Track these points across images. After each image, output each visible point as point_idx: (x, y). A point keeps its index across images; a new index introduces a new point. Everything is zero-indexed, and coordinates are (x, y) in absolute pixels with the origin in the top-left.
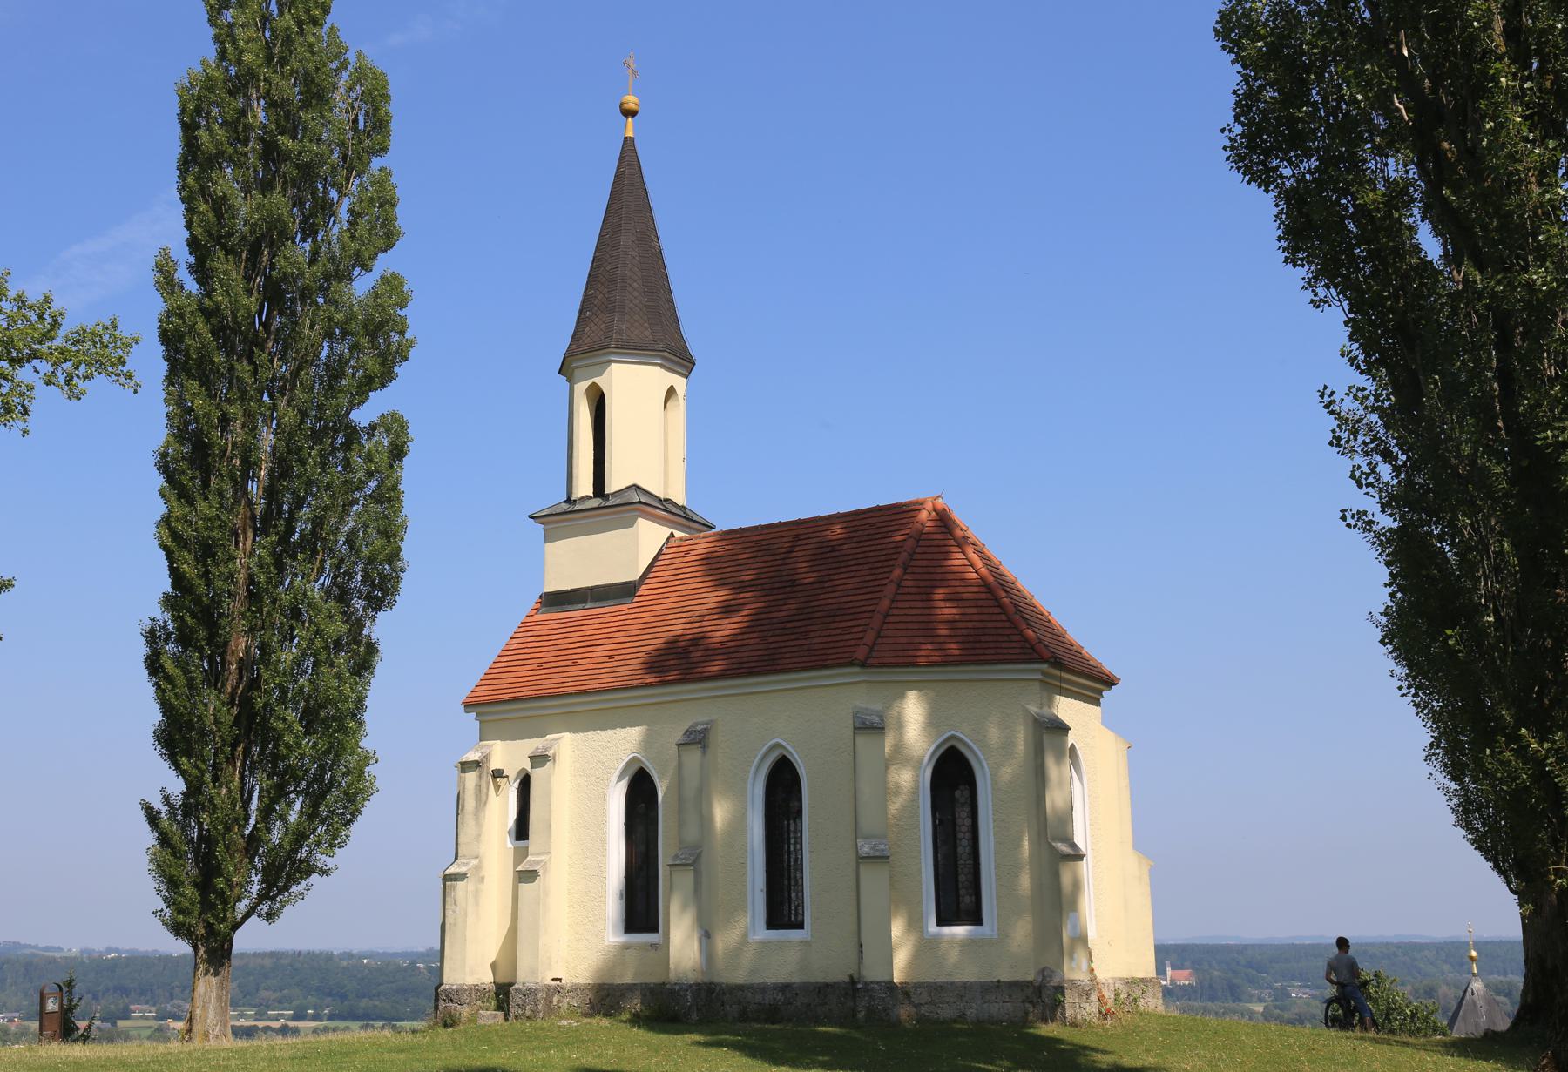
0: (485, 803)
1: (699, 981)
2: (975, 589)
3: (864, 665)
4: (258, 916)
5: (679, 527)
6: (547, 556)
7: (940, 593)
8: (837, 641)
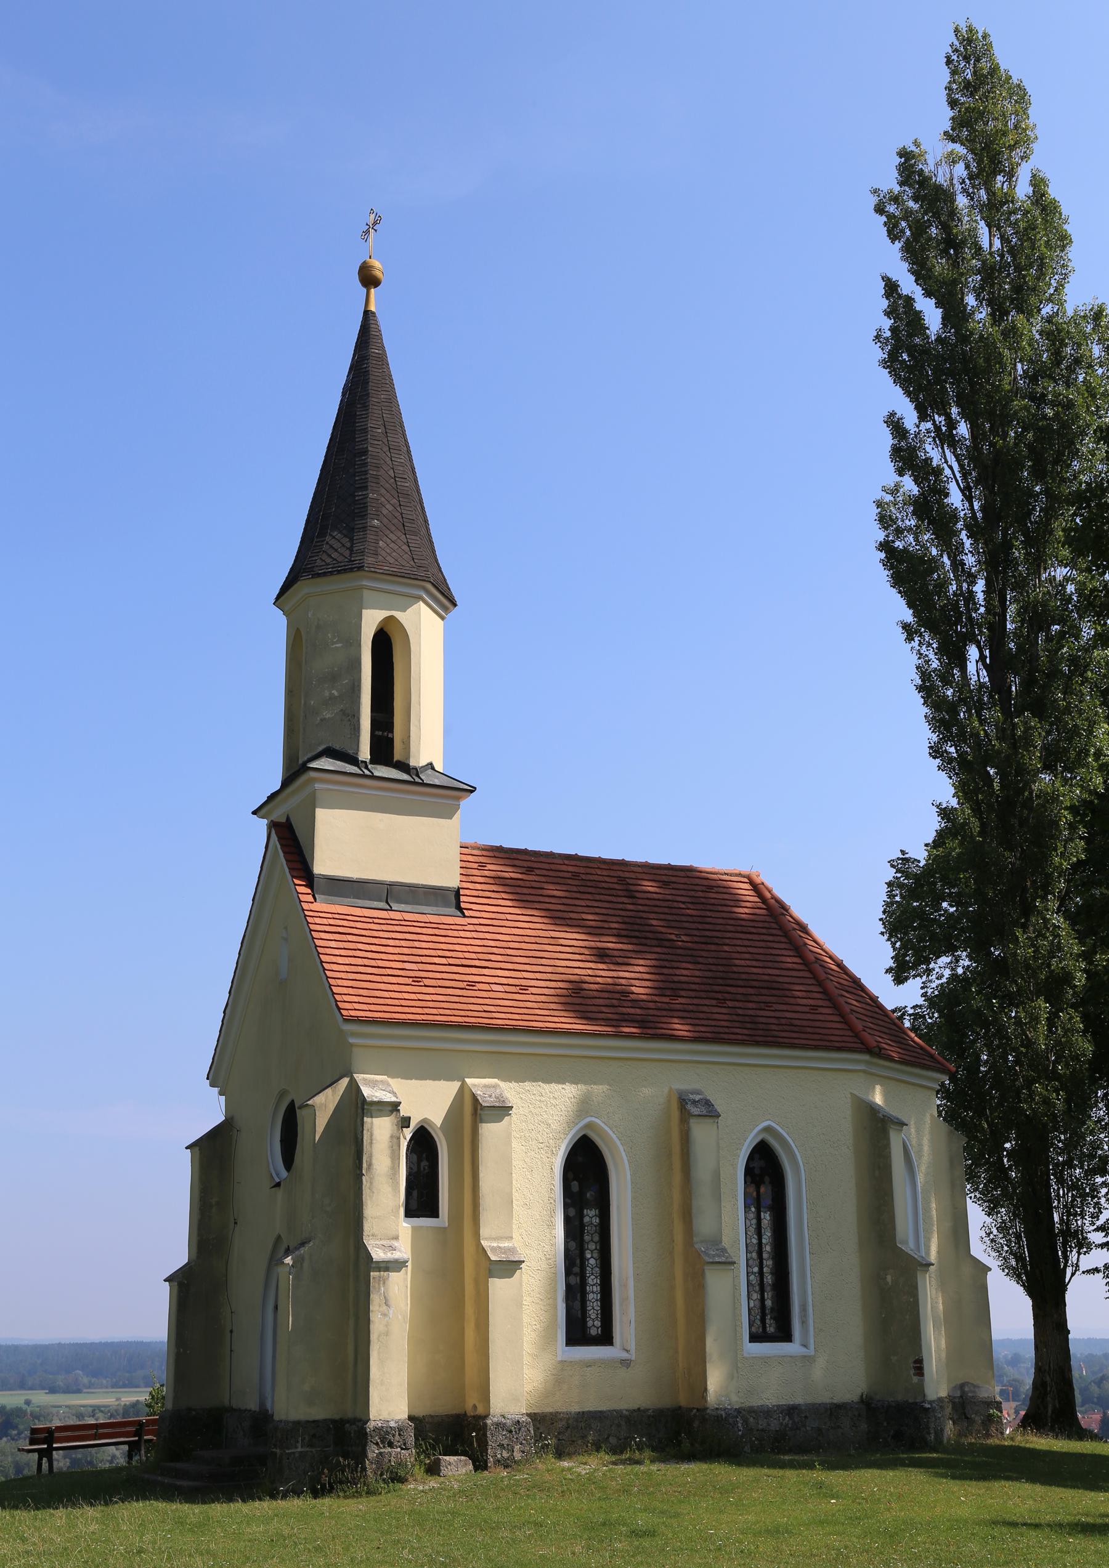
8: (439, 957)
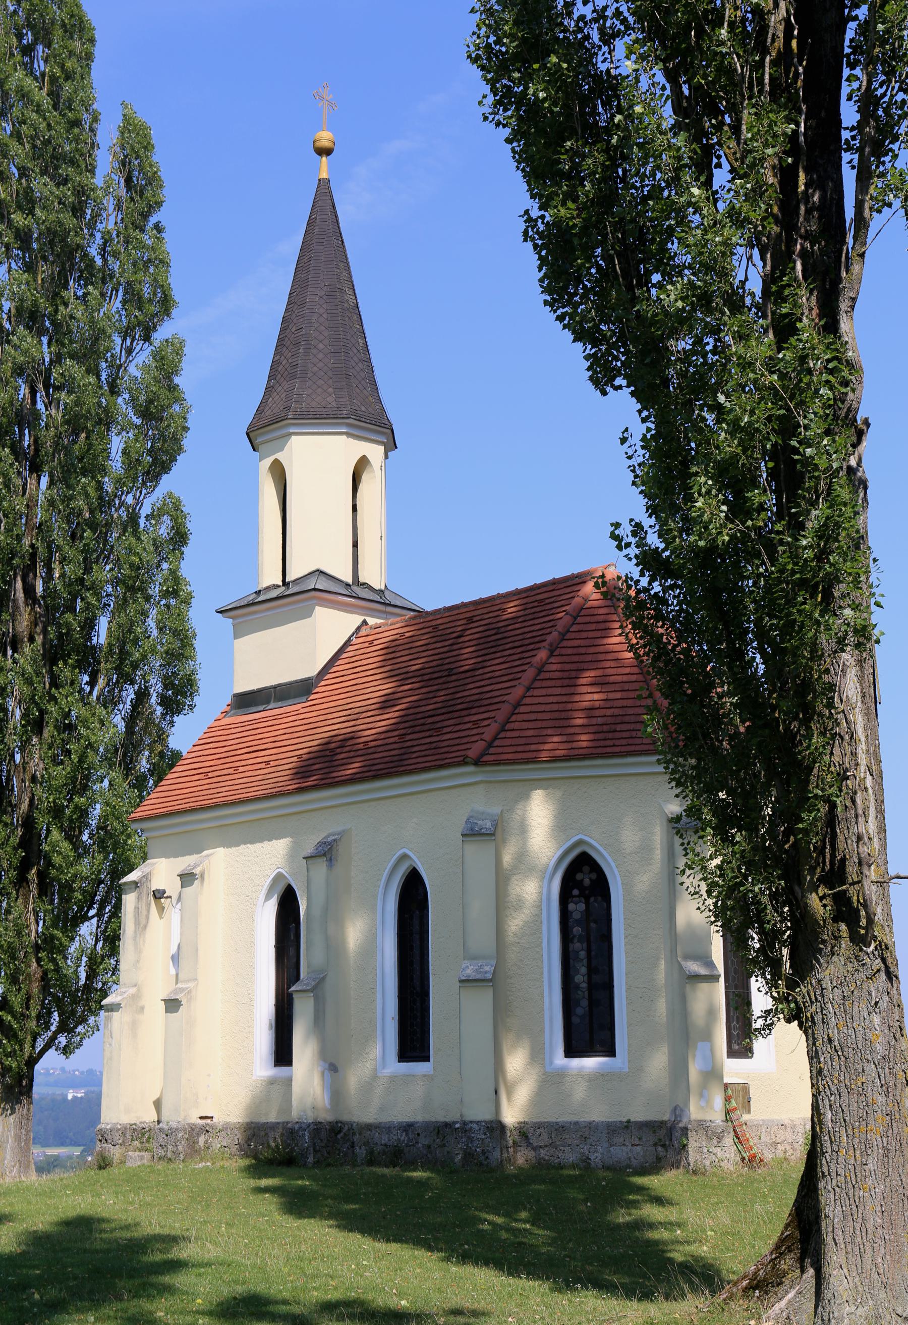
0: (145, 927)
1: (320, 1120)
2: (627, 670)
3: (477, 762)
4: (56, 1050)
5: (376, 614)
6: (238, 657)
7: (588, 676)
